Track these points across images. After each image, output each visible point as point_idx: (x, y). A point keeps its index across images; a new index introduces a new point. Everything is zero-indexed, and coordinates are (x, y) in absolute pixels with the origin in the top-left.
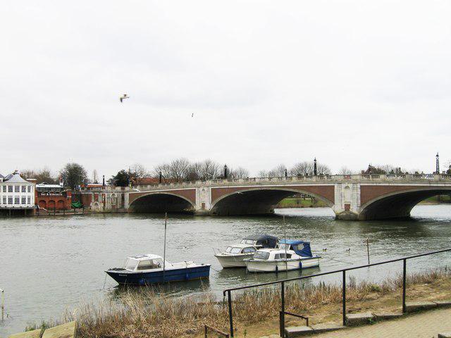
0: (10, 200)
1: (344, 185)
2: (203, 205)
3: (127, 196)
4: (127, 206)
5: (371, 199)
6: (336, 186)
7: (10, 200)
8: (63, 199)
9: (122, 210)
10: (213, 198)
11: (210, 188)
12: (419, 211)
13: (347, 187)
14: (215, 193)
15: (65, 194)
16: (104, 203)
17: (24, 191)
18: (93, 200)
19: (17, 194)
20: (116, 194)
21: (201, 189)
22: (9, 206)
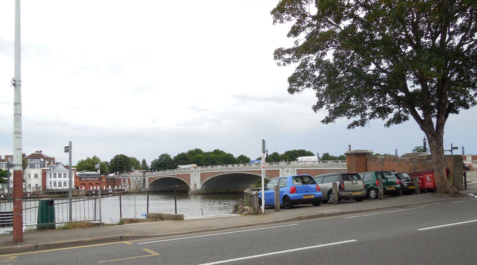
0: (55, 183)
1: (286, 169)
2: (195, 185)
3: (147, 179)
4: (147, 186)
5: (354, 209)
6: (280, 169)
7: (55, 183)
8: (99, 182)
9: (143, 190)
10: (202, 180)
11: (200, 172)
12: (353, 199)
13: (288, 171)
14: (203, 176)
15: (100, 179)
16: (129, 184)
17: (60, 176)
18: (122, 183)
19: (60, 179)
20: (139, 178)
21: (194, 173)
22: (54, 188)
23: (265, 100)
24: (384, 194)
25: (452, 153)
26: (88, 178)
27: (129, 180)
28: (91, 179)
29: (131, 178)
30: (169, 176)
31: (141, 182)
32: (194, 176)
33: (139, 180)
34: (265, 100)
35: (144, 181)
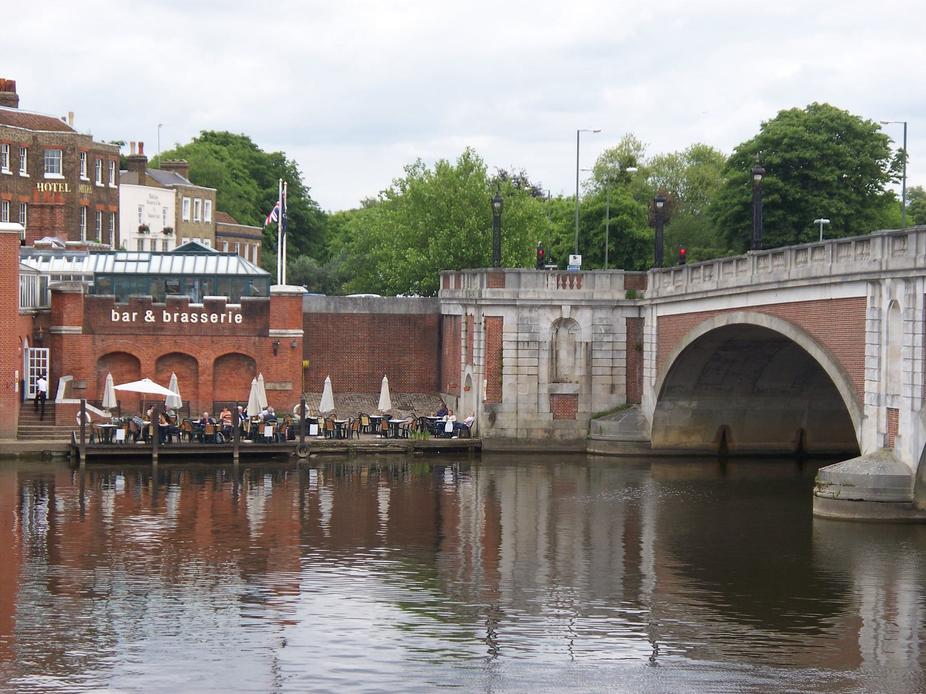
8: (247, 345)
23: (516, 505)
24: (475, 452)
25: (639, 315)
26: (158, 314)
27: (495, 327)
28: (185, 318)
29: (510, 318)
30: (739, 318)
31: (602, 359)
32: (884, 319)
33: (584, 333)
34: (516, 505)
35: (635, 348)
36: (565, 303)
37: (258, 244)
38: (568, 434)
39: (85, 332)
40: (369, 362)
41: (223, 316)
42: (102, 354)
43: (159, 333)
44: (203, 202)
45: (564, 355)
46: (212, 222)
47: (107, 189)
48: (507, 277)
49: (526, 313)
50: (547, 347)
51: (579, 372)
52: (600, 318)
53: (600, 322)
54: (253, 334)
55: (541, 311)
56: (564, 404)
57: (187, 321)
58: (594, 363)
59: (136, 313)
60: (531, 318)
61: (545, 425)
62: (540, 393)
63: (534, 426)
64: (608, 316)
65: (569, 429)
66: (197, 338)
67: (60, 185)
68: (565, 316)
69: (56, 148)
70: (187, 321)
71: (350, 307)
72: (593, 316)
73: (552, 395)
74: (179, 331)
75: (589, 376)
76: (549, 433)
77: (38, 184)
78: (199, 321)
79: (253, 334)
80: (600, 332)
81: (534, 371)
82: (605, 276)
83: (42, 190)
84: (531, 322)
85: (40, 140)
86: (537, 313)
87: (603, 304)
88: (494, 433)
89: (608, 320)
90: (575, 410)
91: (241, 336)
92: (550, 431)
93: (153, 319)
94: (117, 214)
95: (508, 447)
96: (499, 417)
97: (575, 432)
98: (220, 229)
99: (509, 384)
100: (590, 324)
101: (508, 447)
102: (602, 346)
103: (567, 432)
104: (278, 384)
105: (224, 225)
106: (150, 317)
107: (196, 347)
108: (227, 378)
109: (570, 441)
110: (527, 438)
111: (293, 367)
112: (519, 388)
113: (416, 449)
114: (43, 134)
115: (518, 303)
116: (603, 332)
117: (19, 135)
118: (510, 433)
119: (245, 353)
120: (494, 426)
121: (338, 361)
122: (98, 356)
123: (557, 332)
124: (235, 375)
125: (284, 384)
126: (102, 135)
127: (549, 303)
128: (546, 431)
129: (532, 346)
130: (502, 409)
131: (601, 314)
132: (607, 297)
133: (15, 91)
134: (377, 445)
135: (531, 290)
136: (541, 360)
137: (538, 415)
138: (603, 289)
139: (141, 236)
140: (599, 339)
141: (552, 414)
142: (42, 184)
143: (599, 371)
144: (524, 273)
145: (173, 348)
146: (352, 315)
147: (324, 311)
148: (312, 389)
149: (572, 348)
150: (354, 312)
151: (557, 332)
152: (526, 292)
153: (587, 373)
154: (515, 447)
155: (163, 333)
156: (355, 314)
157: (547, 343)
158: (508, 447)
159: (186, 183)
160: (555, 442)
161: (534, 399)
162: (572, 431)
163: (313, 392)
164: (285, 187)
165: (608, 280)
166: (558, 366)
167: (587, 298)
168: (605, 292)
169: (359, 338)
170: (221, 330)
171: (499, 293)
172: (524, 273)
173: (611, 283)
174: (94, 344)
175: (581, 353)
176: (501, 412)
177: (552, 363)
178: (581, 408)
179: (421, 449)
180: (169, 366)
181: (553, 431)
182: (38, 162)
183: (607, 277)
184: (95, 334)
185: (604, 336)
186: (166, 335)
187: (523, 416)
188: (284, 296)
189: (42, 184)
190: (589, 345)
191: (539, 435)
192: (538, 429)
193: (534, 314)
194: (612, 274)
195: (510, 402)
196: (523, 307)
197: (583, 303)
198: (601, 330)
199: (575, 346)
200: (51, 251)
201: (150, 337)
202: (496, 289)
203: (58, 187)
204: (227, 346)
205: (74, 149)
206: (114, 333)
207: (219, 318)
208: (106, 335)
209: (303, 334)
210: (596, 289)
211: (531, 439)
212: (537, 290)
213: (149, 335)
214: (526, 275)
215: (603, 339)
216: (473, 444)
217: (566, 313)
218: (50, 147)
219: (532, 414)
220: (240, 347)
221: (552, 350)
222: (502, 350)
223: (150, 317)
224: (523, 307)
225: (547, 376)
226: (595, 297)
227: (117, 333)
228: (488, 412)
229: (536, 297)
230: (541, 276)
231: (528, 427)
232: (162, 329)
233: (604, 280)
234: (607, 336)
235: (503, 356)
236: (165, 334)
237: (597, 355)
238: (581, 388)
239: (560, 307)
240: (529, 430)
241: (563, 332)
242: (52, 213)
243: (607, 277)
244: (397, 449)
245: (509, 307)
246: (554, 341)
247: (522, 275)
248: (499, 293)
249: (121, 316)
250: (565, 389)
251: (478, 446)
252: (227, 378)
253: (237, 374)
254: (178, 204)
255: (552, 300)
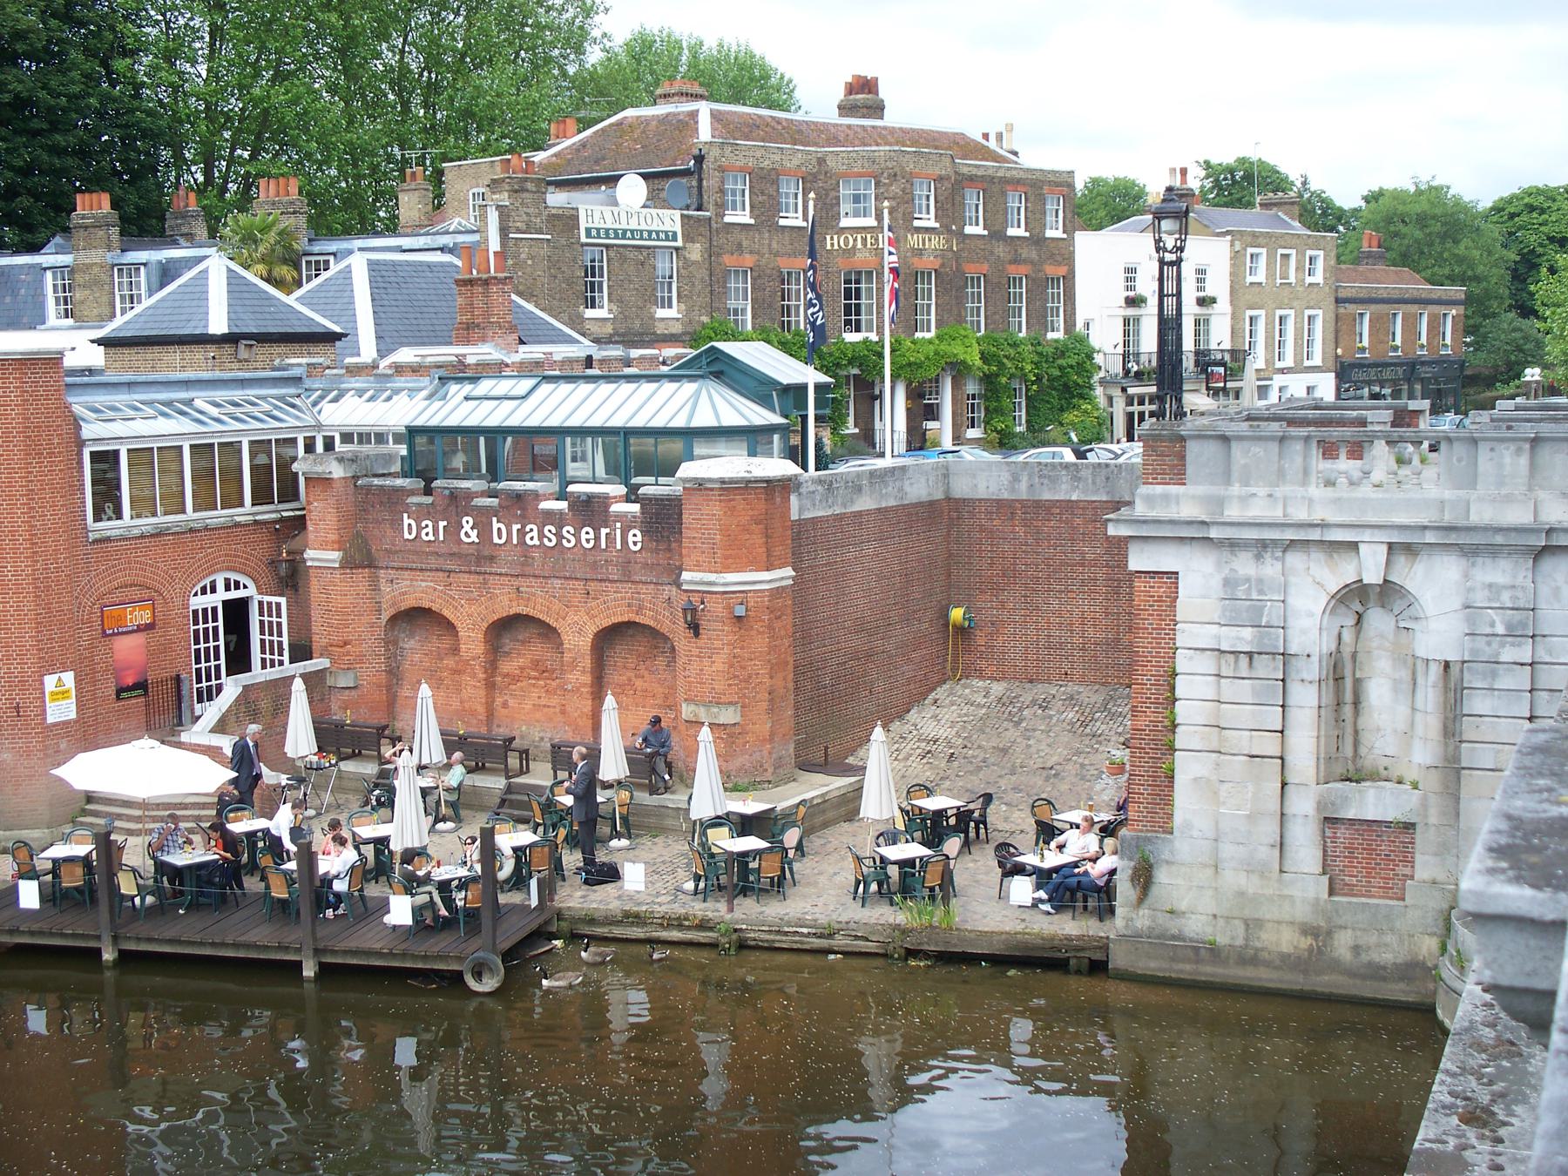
26: (483, 528)
36: (1366, 536)
37: (1454, 312)
38: (1378, 945)
39: (348, 564)
40: (1107, 614)
41: (604, 531)
42: (392, 611)
43: (488, 570)
44: (1301, 254)
45: (1380, 693)
46: (1326, 283)
47: (1037, 240)
48: (1193, 448)
49: (1244, 565)
50: (1311, 670)
51: (1423, 754)
52: (1490, 586)
53: (1490, 600)
54: (666, 580)
55: (1295, 559)
56: (1370, 850)
57: (536, 542)
58: (1468, 729)
59: (445, 523)
60: (1260, 581)
61: (1302, 913)
62: (1289, 811)
63: (1267, 912)
64: (1519, 580)
65: (1381, 932)
66: (557, 583)
67: (869, 236)
68: (1373, 577)
69: (861, 175)
70: (536, 542)
71: (1064, 486)
72: (1466, 576)
73: (1330, 821)
74: (523, 565)
75: (1452, 770)
76: (1316, 936)
77: (828, 237)
78: (559, 543)
79: (666, 580)
80: (1488, 630)
81: (1270, 745)
82: (1512, 447)
83: (836, 247)
84: (1261, 592)
85: (831, 163)
86: (1279, 565)
87: (1499, 539)
88: (1147, 923)
89: (1520, 594)
90: (1407, 871)
91: (641, 582)
92: (1319, 933)
93: (474, 537)
94: (1069, 279)
95: (1185, 970)
96: (1162, 876)
97: (1401, 941)
98: (1342, 294)
99: (1195, 779)
100: (1457, 603)
101: (1188, 967)
102: (1494, 675)
103: (1373, 939)
104: (702, 709)
105: (1351, 288)
106: (469, 532)
107: (557, 606)
108: (630, 680)
109: (1384, 968)
110: (1247, 946)
111: (743, 668)
112: (1223, 794)
113: (911, 953)
114: (837, 154)
115: (1214, 533)
116: (1500, 629)
117: (777, 158)
118: (1196, 926)
119: (652, 623)
120: (1150, 900)
121: (1037, 609)
122: (385, 616)
123: (1359, 622)
124: (646, 673)
125: (716, 710)
126: (1035, 157)
127: (1315, 535)
128: (1307, 930)
129: (1265, 668)
130: (1171, 852)
131: (1498, 572)
132: (1518, 515)
133: (877, 93)
134: (805, 930)
135: (1262, 491)
136: (1293, 713)
137: (1280, 881)
138: (1503, 492)
139: (1131, 312)
140: (1487, 652)
141: (1325, 879)
142: (835, 237)
143: (1484, 757)
144: (1240, 438)
145: (515, 604)
146: (1069, 505)
147: (1006, 495)
148: (981, 670)
149: (1405, 674)
150: (1074, 498)
151: (1359, 622)
152: (1245, 500)
153: (1446, 759)
154: (1208, 969)
155: (493, 570)
156: (1076, 501)
157: (1315, 659)
158: (1188, 967)
159: (1293, 228)
160: (1336, 966)
161: (1270, 829)
162: (1389, 938)
163: (981, 677)
164: (811, 204)
165: (1524, 461)
166: (1360, 727)
167: (1448, 518)
168: (1508, 499)
169: (1084, 559)
170: (602, 566)
171: (1166, 498)
172: (1240, 438)
173: (1533, 466)
174: (375, 587)
175: (1429, 695)
176: (1167, 862)
177: (1339, 720)
178: (1425, 867)
179: (925, 955)
180: (523, 642)
181: (1329, 933)
182: (828, 201)
183: (1519, 451)
184: (376, 567)
185: (1503, 645)
186: (501, 574)
187: (1234, 879)
188: (712, 489)
189: (835, 237)
190: (1455, 670)
191: (1286, 941)
192: (1279, 922)
193: (1271, 568)
194: (1536, 441)
195: (1195, 833)
196: (1233, 545)
197: (1430, 538)
198: (1492, 625)
199: (1413, 666)
200: (372, 378)
201: (474, 578)
202: (1159, 489)
203: (864, 240)
204: (614, 607)
205: (895, 175)
206: (410, 565)
207: (597, 538)
208: (397, 569)
209: (793, 578)
210: (1481, 490)
211: (1257, 950)
212: (1279, 492)
213: (470, 572)
214: (1246, 444)
215: (1498, 654)
216: (1083, 949)
217: (1371, 566)
218: (846, 176)
219: (1262, 875)
220: (640, 609)
221: (1339, 679)
222: (1174, 674)
223: (469, 532)
224: (1233, 545)
225: (1313, 763)
226: (1475, 518)
227: (414, 566)
228: (1131, 859)
229: (1277, 514)
230: (1298, 447)
231: (1247, 913)
232: (492, 559)
233: (1507, 460)
234: (1513, 645)
235: (1178, 693)
236: (499, 571)
237: (1478, 704)
238: (1425, 798)
239: (1354, 546)
240: (1253, 925)
241: (1379, 621)
242: (486, 294)
243: (1519, 451)
244: (862, 946)
245: (1196, 545)
246: (1347, 651)
247: (1234, 444)
248: (1166, 498)
249: (420, 529)
250: (1373, 803)
251: (1098, 956)
252: (630, 680)
253: (651, 672)
254: (1236, 257)
255: (1323, 525)
